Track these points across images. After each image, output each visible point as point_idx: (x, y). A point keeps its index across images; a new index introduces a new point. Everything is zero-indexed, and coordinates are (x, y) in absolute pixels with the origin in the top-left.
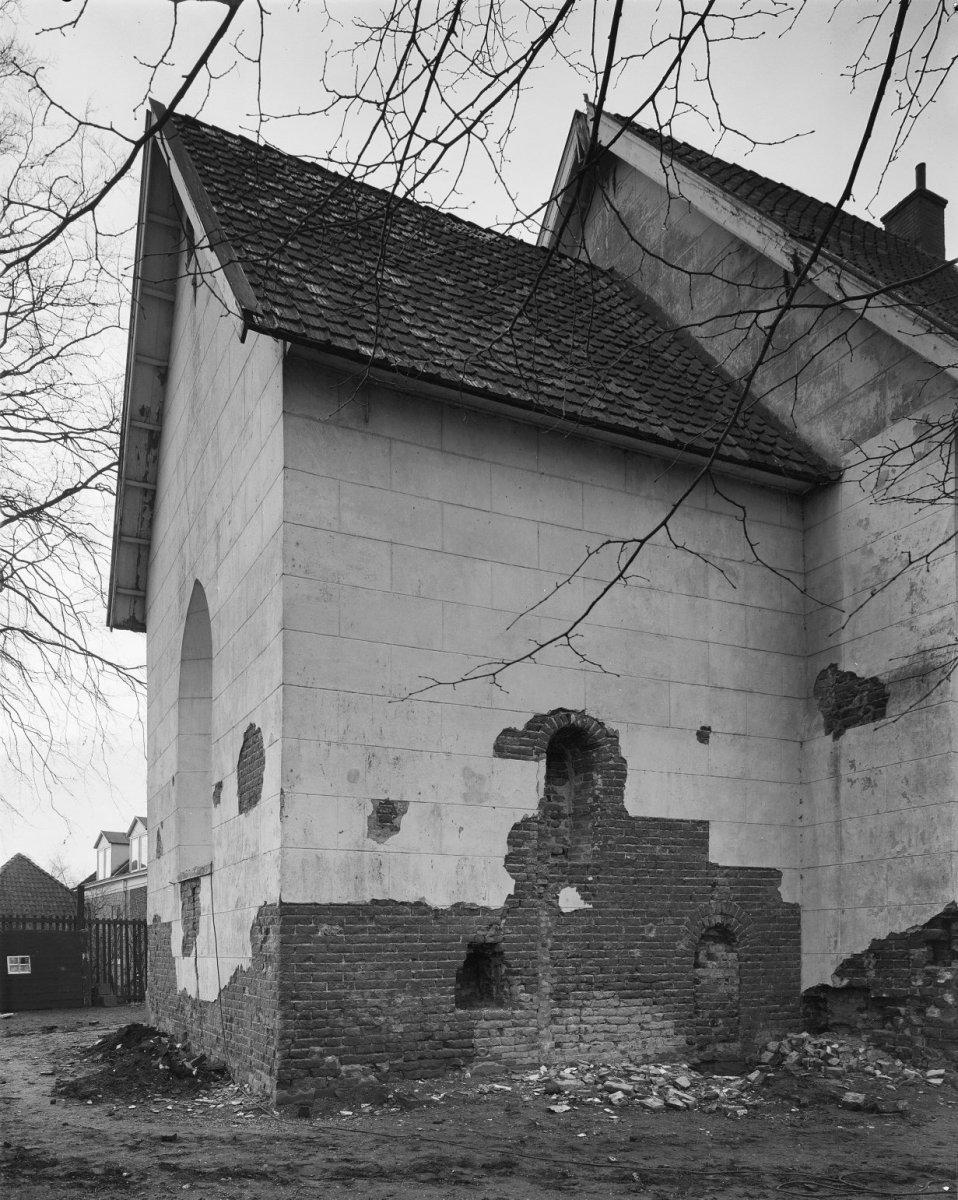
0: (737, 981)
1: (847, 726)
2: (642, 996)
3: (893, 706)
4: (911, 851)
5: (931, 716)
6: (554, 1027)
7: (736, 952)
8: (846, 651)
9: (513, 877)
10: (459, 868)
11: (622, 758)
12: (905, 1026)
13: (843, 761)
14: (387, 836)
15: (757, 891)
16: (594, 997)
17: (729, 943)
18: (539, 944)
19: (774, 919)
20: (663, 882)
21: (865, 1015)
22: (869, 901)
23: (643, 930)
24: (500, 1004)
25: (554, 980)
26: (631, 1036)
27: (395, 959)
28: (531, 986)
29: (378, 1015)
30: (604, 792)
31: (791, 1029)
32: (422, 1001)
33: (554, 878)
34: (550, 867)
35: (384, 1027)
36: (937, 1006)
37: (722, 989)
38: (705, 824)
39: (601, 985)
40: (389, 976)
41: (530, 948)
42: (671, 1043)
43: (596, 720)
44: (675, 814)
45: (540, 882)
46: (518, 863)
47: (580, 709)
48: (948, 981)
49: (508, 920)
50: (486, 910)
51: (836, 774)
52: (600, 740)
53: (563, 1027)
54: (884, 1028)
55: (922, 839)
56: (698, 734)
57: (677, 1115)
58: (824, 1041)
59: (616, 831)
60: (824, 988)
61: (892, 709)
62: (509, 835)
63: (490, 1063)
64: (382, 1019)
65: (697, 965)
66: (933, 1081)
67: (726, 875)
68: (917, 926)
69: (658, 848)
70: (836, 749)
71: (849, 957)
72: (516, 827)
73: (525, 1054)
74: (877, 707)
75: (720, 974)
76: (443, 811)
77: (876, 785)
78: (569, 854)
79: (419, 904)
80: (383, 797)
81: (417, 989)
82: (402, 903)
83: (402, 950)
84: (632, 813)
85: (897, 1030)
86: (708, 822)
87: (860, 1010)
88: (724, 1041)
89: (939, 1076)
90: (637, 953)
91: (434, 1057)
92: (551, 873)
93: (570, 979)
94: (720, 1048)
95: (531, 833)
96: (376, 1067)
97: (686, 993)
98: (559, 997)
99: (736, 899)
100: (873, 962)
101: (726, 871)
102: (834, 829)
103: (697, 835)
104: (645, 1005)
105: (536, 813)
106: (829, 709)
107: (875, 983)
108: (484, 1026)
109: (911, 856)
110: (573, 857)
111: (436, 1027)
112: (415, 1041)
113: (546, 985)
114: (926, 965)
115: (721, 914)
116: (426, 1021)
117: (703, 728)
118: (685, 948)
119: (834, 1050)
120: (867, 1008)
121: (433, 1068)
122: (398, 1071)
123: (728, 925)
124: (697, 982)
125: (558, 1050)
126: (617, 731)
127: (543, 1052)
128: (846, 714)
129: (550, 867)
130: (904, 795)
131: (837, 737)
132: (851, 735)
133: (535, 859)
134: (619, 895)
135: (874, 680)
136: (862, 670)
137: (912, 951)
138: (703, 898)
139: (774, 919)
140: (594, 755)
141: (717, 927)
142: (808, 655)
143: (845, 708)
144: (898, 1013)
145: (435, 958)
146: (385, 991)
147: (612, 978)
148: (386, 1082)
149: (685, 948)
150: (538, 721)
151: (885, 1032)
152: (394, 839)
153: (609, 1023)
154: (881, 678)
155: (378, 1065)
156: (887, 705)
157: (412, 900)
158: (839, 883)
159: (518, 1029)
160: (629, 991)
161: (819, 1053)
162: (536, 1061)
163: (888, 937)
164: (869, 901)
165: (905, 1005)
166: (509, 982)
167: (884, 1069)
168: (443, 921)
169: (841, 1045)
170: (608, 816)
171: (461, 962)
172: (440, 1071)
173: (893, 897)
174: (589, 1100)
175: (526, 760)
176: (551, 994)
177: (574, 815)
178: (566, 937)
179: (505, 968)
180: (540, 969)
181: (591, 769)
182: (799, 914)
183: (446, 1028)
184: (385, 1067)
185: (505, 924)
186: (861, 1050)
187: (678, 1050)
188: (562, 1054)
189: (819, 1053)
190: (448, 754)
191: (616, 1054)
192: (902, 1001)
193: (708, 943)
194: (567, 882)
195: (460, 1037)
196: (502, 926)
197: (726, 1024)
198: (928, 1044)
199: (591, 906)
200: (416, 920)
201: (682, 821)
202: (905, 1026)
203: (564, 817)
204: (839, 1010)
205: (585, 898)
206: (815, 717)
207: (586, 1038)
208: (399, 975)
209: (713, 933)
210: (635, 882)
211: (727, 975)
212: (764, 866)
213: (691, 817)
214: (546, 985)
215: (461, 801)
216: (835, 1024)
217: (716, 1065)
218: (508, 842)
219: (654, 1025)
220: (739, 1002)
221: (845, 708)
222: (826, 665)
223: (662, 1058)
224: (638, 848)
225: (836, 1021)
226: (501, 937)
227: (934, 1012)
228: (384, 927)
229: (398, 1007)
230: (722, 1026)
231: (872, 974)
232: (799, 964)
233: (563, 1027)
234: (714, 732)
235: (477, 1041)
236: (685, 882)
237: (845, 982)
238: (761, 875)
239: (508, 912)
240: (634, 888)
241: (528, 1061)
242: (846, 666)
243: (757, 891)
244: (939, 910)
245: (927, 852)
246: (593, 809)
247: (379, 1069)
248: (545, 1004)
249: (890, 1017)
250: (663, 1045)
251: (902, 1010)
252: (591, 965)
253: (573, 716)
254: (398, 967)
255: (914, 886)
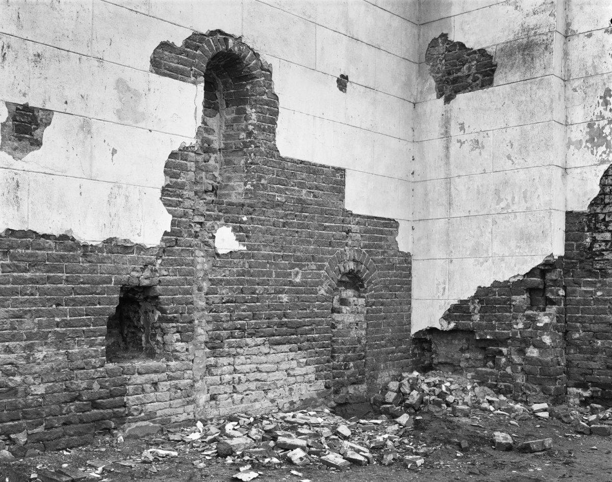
0: (365, 326)
1: (457, 91)
2: (289, 342)
3: (500, 76)
4: (515, 208)
5: (535, 87)
6: (209, 379)
7: (363, 297)
8: (456, 22)
9: (170, 212)
10: (111, 198)
11: (275, 95)
12: (506, 365)
13: (453, 123)
14: (25, 151)
15: (381, 239)
16: (247, 345)
17: (357, 289)
18: (195, 288)
19: (392, 267)
20: (307, 227)
21: (468, 355)
22: (476, 251)
23: (290, 274)
24: (151, 355)
25: (210, 327)
26: (279, 383)
27: (35, 304)
28: (187, 334)
29: (14, 375)
30: (258, 127)
31: (404, 368)
32: (67, 354)
33: (210, 216)
34: (207, 204)
35: (21, 389)
36: (535, 347)
37: (353, 333)
38: (341, 171)
39: (253, 331)
40: (29, 324)
41: (187, 292)
42: (312, 388)
43: (252, 50)
44: (318, 159)
45: (197, 219)
46: (174, 196)
47: (237, 35)
48: (546, 324)
49: (163, 260)
50: (141, 248)
51: (446, 135)
52: (254, 72)
53: (218, 378)
54: (485, 366)
55: (525, 197)
56: (338, 81)
57: (361, 471)
58: (437, 379)
59: (268, 170)
60: (432, 330)
61: (498, 78)
62: (166, 164)
63: (144, 423)
64: (18, 379)
65: (334, 310)
66: (540, 414)
67: (358, 223)
68: (518, 275)
69: (304, 191)
70: (551, 105)
71: (456, 302)
72: (173, 155)
73: (180, 410)
74: (484, 76)
75: (351, 319)
76: (94, 129)
77: (483, 147)
78: (218, 192)
79: (64, 237)
80: (22, 101)
81: (61, 340)
82: (46, 236)
83: (43, 293)
84: (283, 154)
85: (496, 365)
86: (344, 170)
87: (462, 351)
88: (353, 383)
89: (545, 410)
90: (285, 298)
91: (81, 421)
92: (208, 210)
93: (225, 325)
94: (351, 390)
95: (189, 164)
96: (10, 439)
97: (325, 338)
98: (214, 346)
99: (365, 247)
100: (478, 307)
101: (357, 219)
102: (443, 186)
103: (336, 182)
104: (291, 350)
105: (194, 142)
106: (440, 75)
107: (479, 327)
108: (138, 382)
109: (514, 212)
110: (224, 195)
111: (84, 385)
112: (59, 403)
113: (202, 333)
114: (525, 310)
115: (354, 260)
116: (72, 378)
117: (342, 76)
118: (325, 294)
119: (448, 388)
120: (468, 349)
121: (80, 434)
122: (38, 441)
123: (359, 271)
124: (333, 326)
125: (213, 402)
126: (270, 65)
127: (198, 406)
128: (455, 81)
129: (207, 204)
130: (509, 157)
131: (448, 100)
132: (462, 98)
133: (192, 194)
134: (270, 237)
135: (482, 52)
136: (472, 43)
137: (514, 297)
138: (340, 245)
139: (392, 267)
140: (248, 87)
141: (351, 272)
142: (421, 24)
143: (455, 75)
144: (501, 353)
145: (83, 303)
146: (23, 344)
147: (264, 323)
148: (23, 457)
149: (325, 294)
150: (195, 41)
151: (489, 370)
152: (34, 155)
153: (260, 371)
154: (489, 50)
155: (12, 436)
156: (495, 74)
157: (57, 233)
158: (448, 235)
159: (173, 382)
160: (277, 337)
161: (434, 391)
162: (191, 417)
163: (493, 285)
164: (476, 251)
165: (507, 346)
166: (162, 330)
167: (496, 405)
168: (93, 259)
169: (451, 382)
170: (261, 154)
171: (113, 308)
172: (88, 436)
173: (497, 248)
174: (267, 460)
175: (184, 81)
176: (206, 343)
177: (225, 150)
178: (221, 280)
179: (158, 314)
180: (196, 315)
181: (245, 102)
182: (410, 263)
183: (96, 386)
184: (22, 438)
185: (161, 265)
186: (469, 387)
187: (318, 394)
188: (217, 407)
189: (434, 391)
190: (100, 60)
191: (266, 404)
192: (503, 341)
193: (340, 288)
194: (222, 222)
195: (112, 395)
196: (158, 267)
197: (356, 366)
198: (527, 380)
199: (245, 248)
200: (62, 257)
201: (324, 166)
202: (506, 365)
203: (214, 151)
204: (442, 351)
205: (240, 239)
206: (426, 81)
207: (239, 388)
208: (40, 325)
209: (345, 279)
210: (284, 225)
211: (357, 319)
212: (386, 217)
213: (331, 164)
214: (202, 333)
215: (115, 119)
216: (440, 363)
217: (348, 407)
218: (165, 172)
219: (299, 371)
220: (366, 345)
221: (455, 75)
222: (437, 35)
223: (307, 404)
224: (287, 189)
225: (440, 360)
226: (156, 280)
227: (533, 352)
228: (22, 264)
229: (39, 364)
230: (353, 369)
231: (477, 318)
232: (410, 309)
233: (218, 378)
234: (350, 82)
235: (130, 400)
236: (325, 228)
237: (452, 325)
238: (385, 225)
239: (164, 252)
240: (284, 231)
241: (183, 417)
242: (455, 37)
243: (381, 239)
244: (538, 261)
245: (528, 210)
246: (246, 145)
247: (13, 442)
248: (199, 353)
249: (493, 357)
250: (307, 391)
251: (505, 350)
252: (244, 311)
253: (231, 41)
254: (38, 314)
255: (516, 239)
